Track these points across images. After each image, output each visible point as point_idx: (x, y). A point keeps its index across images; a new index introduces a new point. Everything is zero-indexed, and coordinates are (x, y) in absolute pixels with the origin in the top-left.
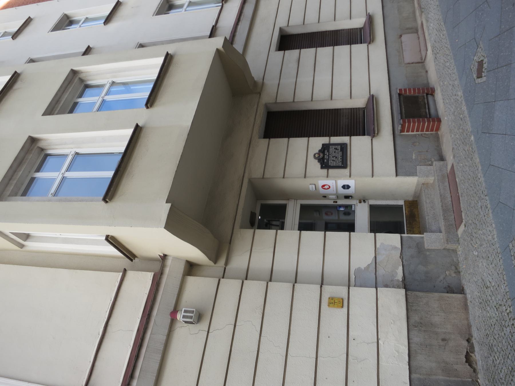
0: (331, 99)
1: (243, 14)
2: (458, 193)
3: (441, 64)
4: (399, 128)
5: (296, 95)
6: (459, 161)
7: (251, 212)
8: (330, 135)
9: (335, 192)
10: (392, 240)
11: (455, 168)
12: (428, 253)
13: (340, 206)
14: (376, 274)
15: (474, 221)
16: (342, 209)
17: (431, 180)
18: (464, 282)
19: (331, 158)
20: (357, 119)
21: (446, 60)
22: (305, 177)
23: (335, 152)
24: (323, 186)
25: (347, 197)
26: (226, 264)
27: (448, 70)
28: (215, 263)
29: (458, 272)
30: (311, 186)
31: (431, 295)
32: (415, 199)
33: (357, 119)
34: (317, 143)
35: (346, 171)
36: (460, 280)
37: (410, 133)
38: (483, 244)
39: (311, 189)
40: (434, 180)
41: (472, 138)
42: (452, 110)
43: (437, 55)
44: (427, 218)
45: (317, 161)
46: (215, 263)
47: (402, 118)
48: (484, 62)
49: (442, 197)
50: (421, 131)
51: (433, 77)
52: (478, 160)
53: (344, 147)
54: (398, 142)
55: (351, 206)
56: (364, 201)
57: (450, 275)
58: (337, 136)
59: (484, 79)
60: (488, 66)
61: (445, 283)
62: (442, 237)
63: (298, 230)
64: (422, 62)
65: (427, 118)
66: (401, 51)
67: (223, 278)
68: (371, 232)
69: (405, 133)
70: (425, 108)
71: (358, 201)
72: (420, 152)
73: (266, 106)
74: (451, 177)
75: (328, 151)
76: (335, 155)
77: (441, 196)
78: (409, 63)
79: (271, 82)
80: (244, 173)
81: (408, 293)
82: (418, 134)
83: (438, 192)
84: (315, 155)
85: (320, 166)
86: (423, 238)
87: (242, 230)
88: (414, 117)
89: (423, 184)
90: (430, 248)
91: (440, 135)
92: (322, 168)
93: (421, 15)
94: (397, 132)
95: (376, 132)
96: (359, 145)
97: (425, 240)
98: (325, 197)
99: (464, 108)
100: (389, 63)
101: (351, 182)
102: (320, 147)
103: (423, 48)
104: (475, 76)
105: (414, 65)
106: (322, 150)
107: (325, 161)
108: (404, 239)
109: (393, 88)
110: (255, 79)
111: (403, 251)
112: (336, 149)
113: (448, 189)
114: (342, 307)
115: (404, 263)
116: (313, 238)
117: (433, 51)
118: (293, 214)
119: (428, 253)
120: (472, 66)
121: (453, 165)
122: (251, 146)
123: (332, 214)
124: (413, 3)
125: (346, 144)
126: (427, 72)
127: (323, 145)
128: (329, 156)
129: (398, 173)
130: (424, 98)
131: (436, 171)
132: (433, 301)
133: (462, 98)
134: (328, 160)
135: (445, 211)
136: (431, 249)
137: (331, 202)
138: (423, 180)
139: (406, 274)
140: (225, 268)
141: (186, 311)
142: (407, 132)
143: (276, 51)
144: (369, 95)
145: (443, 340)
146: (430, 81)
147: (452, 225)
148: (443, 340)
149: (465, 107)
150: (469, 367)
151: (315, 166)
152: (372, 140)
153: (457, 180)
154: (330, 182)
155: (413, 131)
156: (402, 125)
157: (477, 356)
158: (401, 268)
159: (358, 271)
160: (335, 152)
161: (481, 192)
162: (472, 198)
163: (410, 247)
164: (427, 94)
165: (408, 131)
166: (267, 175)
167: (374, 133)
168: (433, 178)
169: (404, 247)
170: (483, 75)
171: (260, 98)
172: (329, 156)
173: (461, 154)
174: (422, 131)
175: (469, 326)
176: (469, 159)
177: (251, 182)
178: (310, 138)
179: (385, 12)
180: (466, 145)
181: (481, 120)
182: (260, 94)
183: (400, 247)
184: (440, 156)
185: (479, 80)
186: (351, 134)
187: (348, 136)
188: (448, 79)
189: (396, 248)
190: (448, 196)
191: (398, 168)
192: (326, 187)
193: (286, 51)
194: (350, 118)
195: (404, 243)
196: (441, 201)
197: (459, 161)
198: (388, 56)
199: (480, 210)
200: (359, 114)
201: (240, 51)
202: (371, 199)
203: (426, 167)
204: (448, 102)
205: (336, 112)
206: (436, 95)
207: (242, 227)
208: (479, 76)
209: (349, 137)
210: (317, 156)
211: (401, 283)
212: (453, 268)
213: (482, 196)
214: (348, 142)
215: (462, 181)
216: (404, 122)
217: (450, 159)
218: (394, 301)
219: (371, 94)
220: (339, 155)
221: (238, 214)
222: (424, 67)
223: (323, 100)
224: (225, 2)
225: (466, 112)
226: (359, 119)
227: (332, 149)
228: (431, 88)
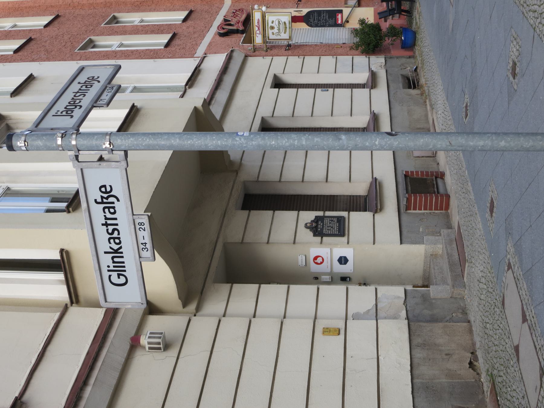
1: (214, 99)
4: (404, 202)
8: (324, 210)
9: (329, 270)
20: (357, 205)
24: (316, 258)
31: (436, 324)
33: (357, 205)
35: (344, 239)
37: (417, 211)
39: (300, 263)
53: (341, 221)
57: (457, 316)
65: (435, 193)
70: (434, 188)
73: (245, 184)
77: (448, 254)
80: (218, 238)
81: (410, 323)
84: (306, 224)
86: (429, 290)
87: (216, 284)
88: (420, 193)
89: (432, 255)
93: (432, 114)
96: (358, 221)
98: (316, 278)
101: (348, 252)
102: (313, 218)
105: (425, 158)
106: (316, 221)
110: (231, 159)
111: (407, 300)
114: (339, 334)
115: (408, 308)
119: (434, 301)
124: (426, 108)
125: (343, 218)
127: (316, 217)
129: (404, 239)
130: (433, 180)
132: (438, 333)
135: (451, 265)
141: (151, 333)
143: (271, 88)
144: (371, 180)
145: (446, 355)
148: (446, 355)
150: (472, 371)
151: (306, 235)
152: (374, 215)
154: (323, 251)
157: (481, 364)
164: (436, 178)
165: (415, 209)
166: (247, 240)
167: (377, 207)
169: (407, 297)
175: (474, 344)
178: (301, 212)
179: (392, 113)
182: (237, 173)
183: (403, 296)
186: (350, 209)
187: (346, 211)
192: (319, 260)
194: (348, 204)
201: (218, 117)
206: (445, 178)
212: (460, 311)
218: (396, 333)
219: (374, 177)
220: (336, 226)
223: (316, 182)
224: (189, 88)
227: (326, 221)
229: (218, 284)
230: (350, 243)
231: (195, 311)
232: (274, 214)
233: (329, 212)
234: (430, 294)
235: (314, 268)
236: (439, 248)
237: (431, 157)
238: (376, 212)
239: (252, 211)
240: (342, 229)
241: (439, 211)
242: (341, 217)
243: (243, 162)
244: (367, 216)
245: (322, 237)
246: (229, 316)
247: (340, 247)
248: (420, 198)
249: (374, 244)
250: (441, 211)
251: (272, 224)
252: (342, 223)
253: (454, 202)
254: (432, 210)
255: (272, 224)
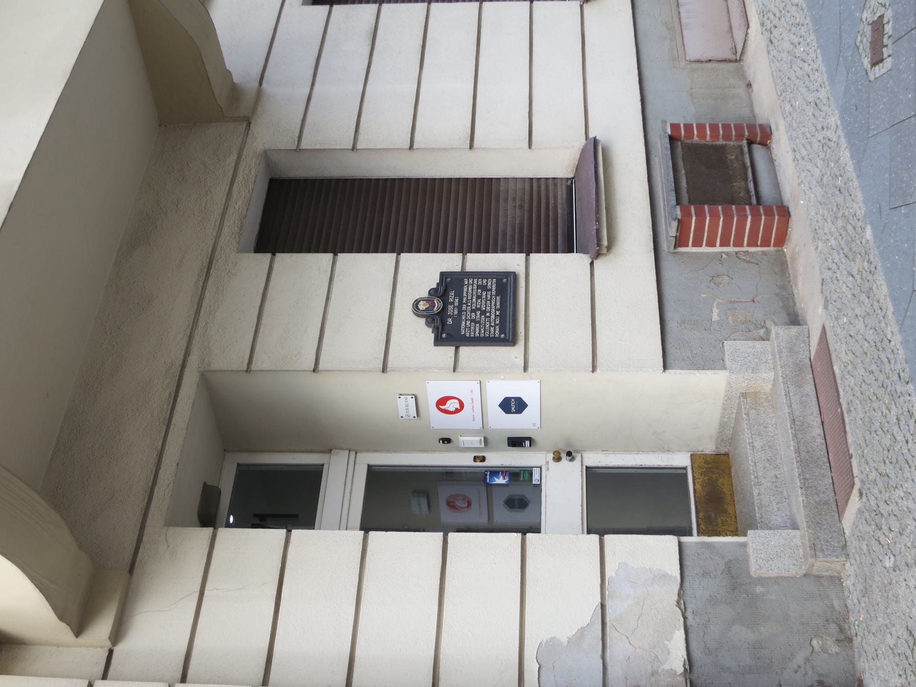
0: (471, 147)
2: (840, 404)
3: (784, 55)
4: (669, 230)
5: (361, 130)
6: (840, 310)
7: (205, 484)
8: (465, 248)
10: (650, 556)
11: (828, 330)
12: (759, 589)
13: (495, 472)
14: (603, 657)
15: (882, 468)
16: (500, 480)
17: (765, 380)
18: (862, 664)
19: (467, 315)
20: (547, 216)
21: (796, 41)
22: (384, 369)
23: (479, 297)
24: (442, 401)
25: (516, 442)
26: (117, 635)
27: (802, 64)
28: (78, 631)
29: (846, 640)
30: (401, 402)
32: (723, 450)
33: (547, 216)
34: (424, 270)
35: (514, 354)
36: (852, 662)
37: (704, 249)
38: (907, 525)
39: (402, 412)
40: (776, 375)
41: (869, 232)
42: (817, 173)
43: (775, 32)
44: (755, 493)
45: (423, 321)
46: (78, 631)
47: (678, 202)
48: (885, 20)
49: (798, 427)
50: (735, 245)
51: (766, 103)
52: (885, 289)
53: (506, 286)
54: (667, 274)
55: (529, 472)
56: (569, 454)
57: (824, 649)
58: (487, 251)
59: (888, 63)
60: (894, 28)
61: (810, 673)
62: (799, 543)
63: (361, 529)
64: (737, 58)
65: (750, 204)
66: (676, 28)
67: (104, 677)
68: (589, 532)
69: (690, 249)
70: (746, 179)
71: (551, 456)
72: (731, 302)
73: (267, 158)
74: (821, 372)
75: (459, 294)
76: (481, 306)
77: (793, 421)
78: (699, 61)
79: (285, 88)
82: (727, 254)
83: (787, 410)
84: (416, 303)
85: (432, 336)
86: (744, 545)
87: (172, 530)
88: (713, 202)
89: (744, 395)
90: (764, 573)
91: (788, 257)
92: (438, 341)
94: (666, 245)
95: (605, 243)
96: (551, 280)
97: (750, 550)
98: (447, 441)
99: (846, 156)
100: (644, 57)
101: (524, 388)
102: (433, 281)
103: (737, 20)
104: (866, 62)
106: (442, 290)
107: (450, 321)
108: (687, 551)
109: (653, 125)
110: (236, 79)
111: (687, 584)
112: (484, 288)
113: (815, 402)
115: (690, 621)
116: (406, 553)
117: (763, 24)
118: (343, 488)
119: (759, 589)
120: (859, 38)
121: (824, 328)
122: (213, 272)
123: (469, 504)
125: (514, 275)
126: (749, 85)
127: (443, 275)
128: (460, 307)
129: (670, 359)
130: (742, 153)
131: (780, 352)
133: (840, 132)
134: (458, 320)
135: (805, 462)
136: (769, 578)
137: (464, 460)
138: (743, 381)
139: (697, 654)
140: (111, 652)
142: (695, 245)
146: (757, 110)
147: (826, 503)
149: (847, 154)
151: (416, 335)
152: (592, 264)
153: (836, 369)
154: (460, 387)
155: (711, 244)
156: (680, 222)
158: (680, 635)
159: (550, 647)
160: (479, 297)
161: (896, 377)
162: (875, 405)
163: (705, 574)
164: (750, 143)
165: (697, 243)
167: (599, 244)
168: (771, 375)
170: (885, 56)
171: (247, 134)
172: (460, 307)
173: (844, 288)
174: (739, 243)
176: (863, 297)
177: (206, 382)
178: (404, 256)
180: (854, 260)
181: (887, 176)
184: (789, 314)
185: (879, 70)
186: (530, 243)
188: (804, 90)
189: (665, 576)
190: (815, 421)
191: (669, 346)
192: (451, 405)
193: (336, 8)
194: (526, 207)
195: (687, 563)
196: (795, 436)
197: (840, 310)
198: (640, 39)
199: (895, 429)
200: (555, 197)
202: (593, 448)
203: (750, 343)
204: (804, 153)
205: (485, 189)
206: (774, 145)
207: (174, 521)
208: (877, 61)
209: (523, 255)
210: (422, 306)
211: (682, 679)
213: (899, 389)
214: (520, 270)
215: (849, 368)
216: (686, 213)
217: (815, 314)
219: (591, 135)
220: (493, 305)
221: (160, 480)
222: (741, 74)
225: (850, 167)
226: (555, 208)
227: (470, 288)
228: (761, 127)
229: (180, 528)
230: (530, 369)
231: (108, 644)
232: (334, 263)
233: (481, 229)
234: (746, 560)
235: (440, 422)
236: (765, 380)
237: (730, 61)
238: (598, 255)
239: (279, 256)
240: (509, 325)
241: (759, 249)
242: (507, 274)
243: (264, 85)
244: (576, 262)
245: (457, 348)
246: (194, 682)
247: (504, 379)
248: (714, 218)
249: (594, 369)
250: (765, 249)
251: (328, 299)
252: (510, 301)
253: (798, 230)
254: (741, 245)
255: (328, 299)
